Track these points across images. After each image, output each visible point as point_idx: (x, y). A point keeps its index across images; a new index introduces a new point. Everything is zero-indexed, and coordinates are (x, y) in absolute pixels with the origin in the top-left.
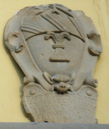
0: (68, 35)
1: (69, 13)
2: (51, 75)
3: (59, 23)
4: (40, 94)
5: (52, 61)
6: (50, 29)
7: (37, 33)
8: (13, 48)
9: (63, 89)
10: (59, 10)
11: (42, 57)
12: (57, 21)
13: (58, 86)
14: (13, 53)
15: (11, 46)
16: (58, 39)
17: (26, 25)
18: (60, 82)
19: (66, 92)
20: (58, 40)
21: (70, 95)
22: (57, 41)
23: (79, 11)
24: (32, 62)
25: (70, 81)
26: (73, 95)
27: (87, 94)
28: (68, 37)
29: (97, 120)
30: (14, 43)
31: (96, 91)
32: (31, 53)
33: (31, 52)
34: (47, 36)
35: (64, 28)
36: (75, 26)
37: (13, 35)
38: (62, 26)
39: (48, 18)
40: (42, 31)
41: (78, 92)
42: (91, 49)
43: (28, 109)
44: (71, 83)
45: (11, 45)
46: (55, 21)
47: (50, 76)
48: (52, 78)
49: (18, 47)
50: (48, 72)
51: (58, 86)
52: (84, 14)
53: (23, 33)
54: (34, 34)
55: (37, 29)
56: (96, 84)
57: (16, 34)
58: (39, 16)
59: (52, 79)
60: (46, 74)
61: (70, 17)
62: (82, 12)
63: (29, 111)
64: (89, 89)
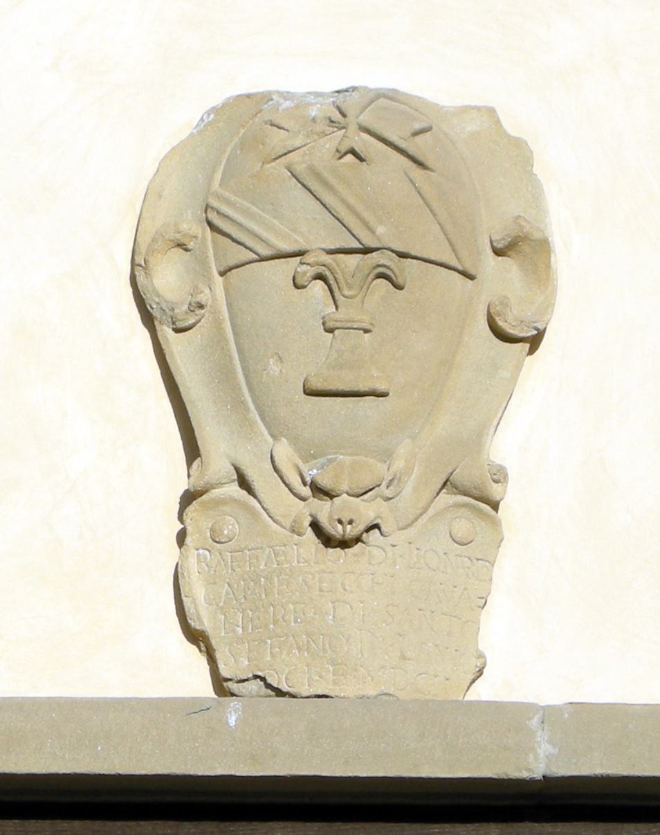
0: (392, 266)
1: (418, 146)
2: (301, 457)
3: (360, 208)
4: (252, 545)
5: (311, 393)
6: (317, 233)
7: (265, 252)
8: (164, 305)
9: (344, 531)
10: (371, 135)
11: (274, 367)
12: (352, 200)
13: (324, 510)
14: (166, 332)
15: (157, 300)
16: (350, 287)
17: (228, 202)
18: (342, 494)
19: (358, 540)
20: (346, 292)
21: (375, 551)
22: (344, 296)
23: (478, 109)
24: (235, 387)
25: (384, 484)
26: (389, 549)
27: (453, 540)
28: (396, 276)
29: (481, 656)
30: (168, 280)
31: (496, 524)
32: (237, 343)
33: (235, 334)
34: (304, 273)
35: (380, 230)
36: (435, 215)
37: (172, 244)
38: (372, 221)
39: (314, 186)
40: (286, 247)
41: (412, 531)
42: (497, 319)
43: (197, 612)
44: (388, 493)
45: (158, 296)
46: (343, 201)
47: (301, 464)
48: (311, 473)
49: (185, 307)
50: (295, 441)
51: (324, 510)
52: (498, 122)
53: (212, 234)
54: (256, 257)
55: (265, 235)
56: (495, 490)
57: (185, 241)
58: (278, 168)
59: (308, 480)
60: (285, 452)
61: (416, 172)
62: (491, 111)
63: (199, 618)
64: (463, 511)
